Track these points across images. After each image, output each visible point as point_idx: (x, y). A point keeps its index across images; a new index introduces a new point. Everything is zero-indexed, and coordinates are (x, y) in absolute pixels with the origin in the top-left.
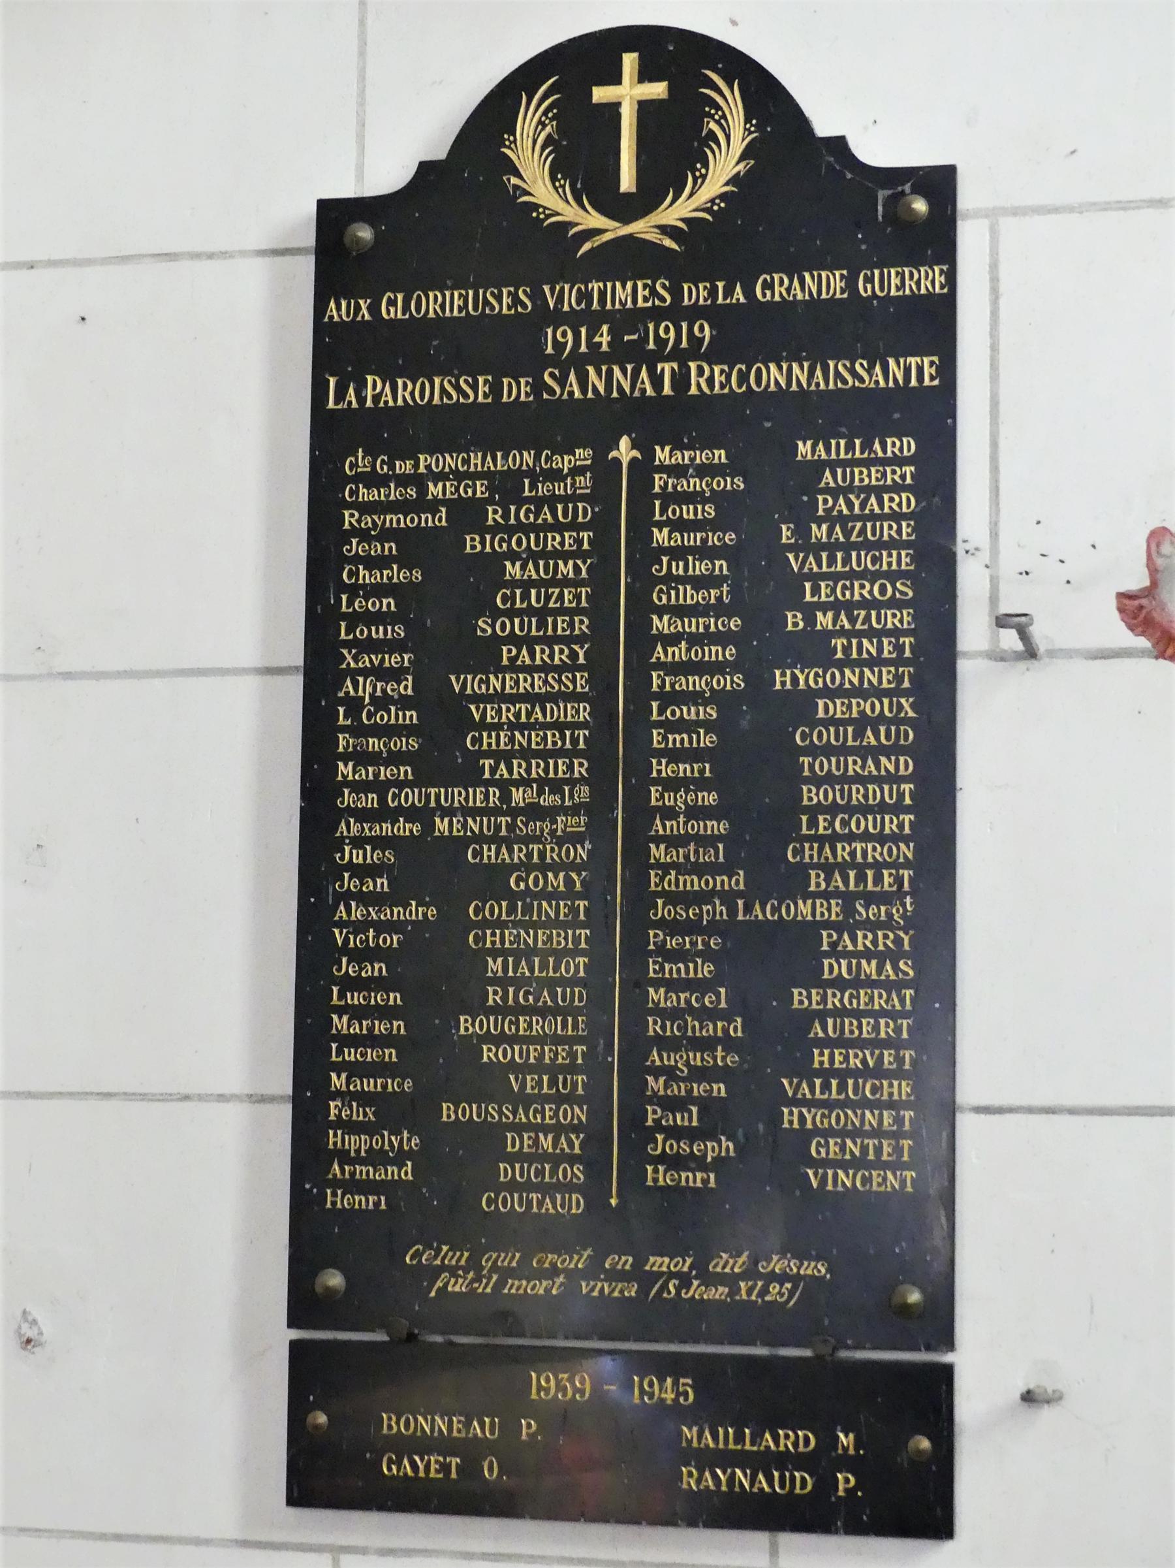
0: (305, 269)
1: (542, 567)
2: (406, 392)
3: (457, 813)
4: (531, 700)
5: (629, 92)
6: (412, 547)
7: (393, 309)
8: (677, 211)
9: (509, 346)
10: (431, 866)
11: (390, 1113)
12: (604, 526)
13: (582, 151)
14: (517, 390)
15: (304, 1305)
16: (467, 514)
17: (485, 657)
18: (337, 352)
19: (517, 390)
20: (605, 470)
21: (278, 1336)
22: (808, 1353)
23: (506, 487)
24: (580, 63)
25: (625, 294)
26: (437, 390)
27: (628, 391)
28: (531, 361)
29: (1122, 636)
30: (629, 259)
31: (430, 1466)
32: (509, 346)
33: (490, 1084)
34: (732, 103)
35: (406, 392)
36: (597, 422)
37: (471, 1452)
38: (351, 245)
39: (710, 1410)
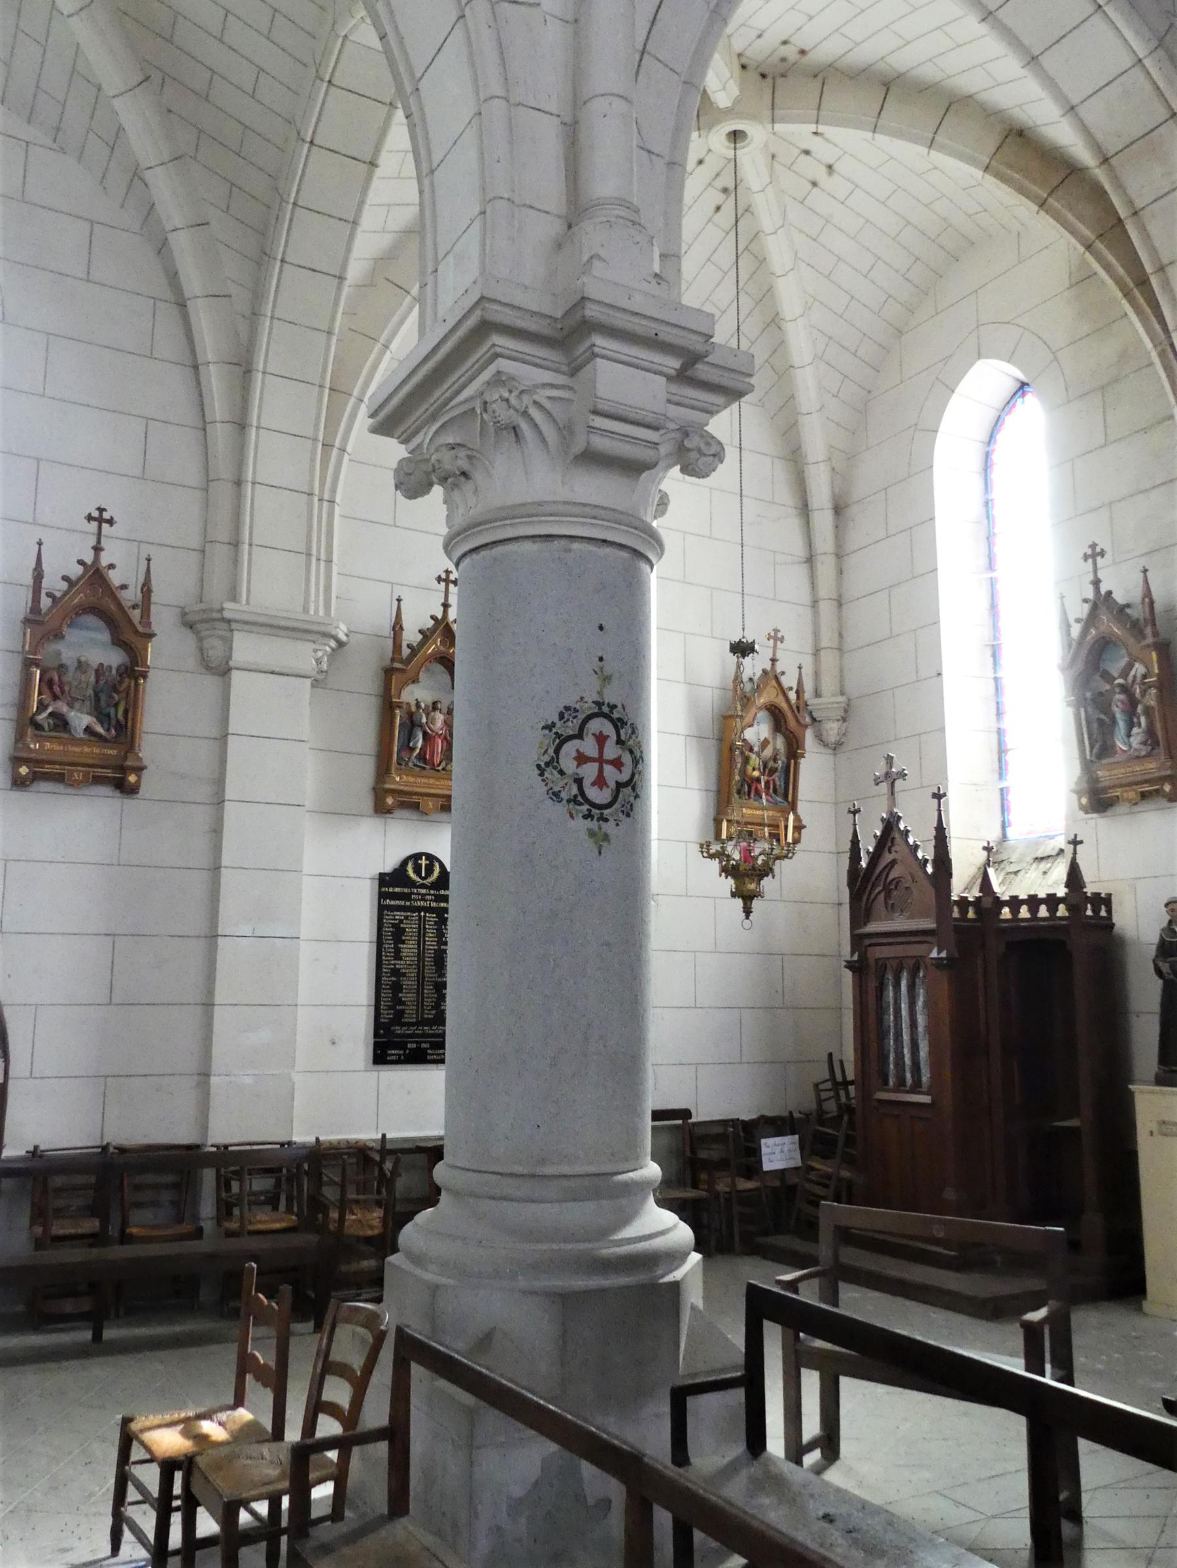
0: (377, 882)
1: (411, 928)
2: (393, 903)
3: (400, 964)
4: (409, 949)
5: (424, 862)
6: (393, 925)
7: (391, 890)
8: (430, 880)
9: (406, 897)
10: (396, 972)
11: (390, 1008)
12: (419, 925)
13: (417, 870)
14: (408, 903)
15: (376, 1035)
16: (401, 921)
17: (403, 942)
18: (382, 896)
19: (408, 903)
20: (420, 916)
21: (372, 1041)
22: (261, 1296)
23: (406, 918)
24: (417, 857)
25: (423, 891)
26: (397, 902)
27: (883, 894)
28: (410, 900)
29: (762, 739)
30: (423, 886)
31: (394, 1058)
32: (406, 897)
33: (403, 1003)
34: (437, 865)
35: (393, 903)
36: (419, 909)
37: (399, 1055)
38: (384, 880)
39: (431, 1048)
